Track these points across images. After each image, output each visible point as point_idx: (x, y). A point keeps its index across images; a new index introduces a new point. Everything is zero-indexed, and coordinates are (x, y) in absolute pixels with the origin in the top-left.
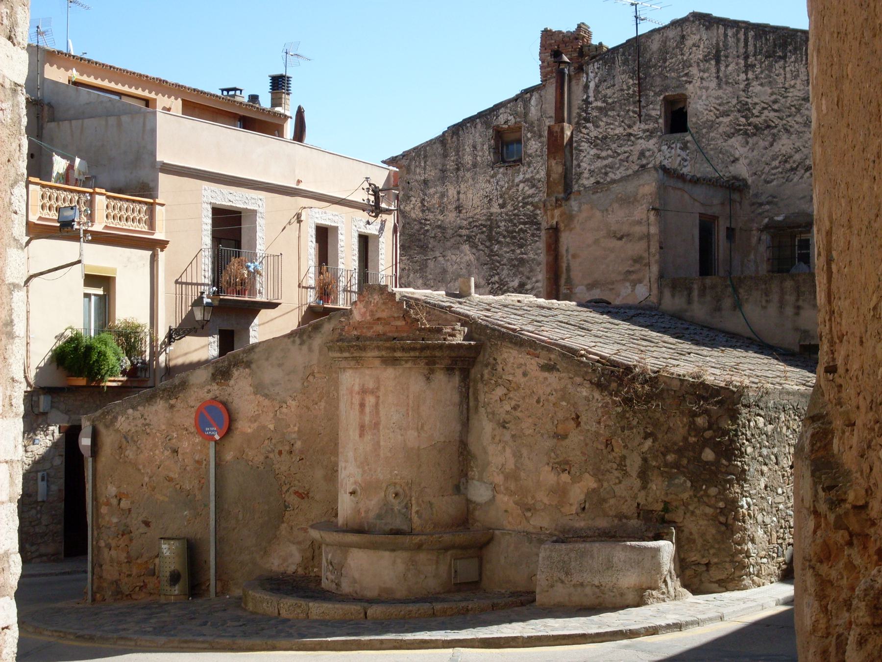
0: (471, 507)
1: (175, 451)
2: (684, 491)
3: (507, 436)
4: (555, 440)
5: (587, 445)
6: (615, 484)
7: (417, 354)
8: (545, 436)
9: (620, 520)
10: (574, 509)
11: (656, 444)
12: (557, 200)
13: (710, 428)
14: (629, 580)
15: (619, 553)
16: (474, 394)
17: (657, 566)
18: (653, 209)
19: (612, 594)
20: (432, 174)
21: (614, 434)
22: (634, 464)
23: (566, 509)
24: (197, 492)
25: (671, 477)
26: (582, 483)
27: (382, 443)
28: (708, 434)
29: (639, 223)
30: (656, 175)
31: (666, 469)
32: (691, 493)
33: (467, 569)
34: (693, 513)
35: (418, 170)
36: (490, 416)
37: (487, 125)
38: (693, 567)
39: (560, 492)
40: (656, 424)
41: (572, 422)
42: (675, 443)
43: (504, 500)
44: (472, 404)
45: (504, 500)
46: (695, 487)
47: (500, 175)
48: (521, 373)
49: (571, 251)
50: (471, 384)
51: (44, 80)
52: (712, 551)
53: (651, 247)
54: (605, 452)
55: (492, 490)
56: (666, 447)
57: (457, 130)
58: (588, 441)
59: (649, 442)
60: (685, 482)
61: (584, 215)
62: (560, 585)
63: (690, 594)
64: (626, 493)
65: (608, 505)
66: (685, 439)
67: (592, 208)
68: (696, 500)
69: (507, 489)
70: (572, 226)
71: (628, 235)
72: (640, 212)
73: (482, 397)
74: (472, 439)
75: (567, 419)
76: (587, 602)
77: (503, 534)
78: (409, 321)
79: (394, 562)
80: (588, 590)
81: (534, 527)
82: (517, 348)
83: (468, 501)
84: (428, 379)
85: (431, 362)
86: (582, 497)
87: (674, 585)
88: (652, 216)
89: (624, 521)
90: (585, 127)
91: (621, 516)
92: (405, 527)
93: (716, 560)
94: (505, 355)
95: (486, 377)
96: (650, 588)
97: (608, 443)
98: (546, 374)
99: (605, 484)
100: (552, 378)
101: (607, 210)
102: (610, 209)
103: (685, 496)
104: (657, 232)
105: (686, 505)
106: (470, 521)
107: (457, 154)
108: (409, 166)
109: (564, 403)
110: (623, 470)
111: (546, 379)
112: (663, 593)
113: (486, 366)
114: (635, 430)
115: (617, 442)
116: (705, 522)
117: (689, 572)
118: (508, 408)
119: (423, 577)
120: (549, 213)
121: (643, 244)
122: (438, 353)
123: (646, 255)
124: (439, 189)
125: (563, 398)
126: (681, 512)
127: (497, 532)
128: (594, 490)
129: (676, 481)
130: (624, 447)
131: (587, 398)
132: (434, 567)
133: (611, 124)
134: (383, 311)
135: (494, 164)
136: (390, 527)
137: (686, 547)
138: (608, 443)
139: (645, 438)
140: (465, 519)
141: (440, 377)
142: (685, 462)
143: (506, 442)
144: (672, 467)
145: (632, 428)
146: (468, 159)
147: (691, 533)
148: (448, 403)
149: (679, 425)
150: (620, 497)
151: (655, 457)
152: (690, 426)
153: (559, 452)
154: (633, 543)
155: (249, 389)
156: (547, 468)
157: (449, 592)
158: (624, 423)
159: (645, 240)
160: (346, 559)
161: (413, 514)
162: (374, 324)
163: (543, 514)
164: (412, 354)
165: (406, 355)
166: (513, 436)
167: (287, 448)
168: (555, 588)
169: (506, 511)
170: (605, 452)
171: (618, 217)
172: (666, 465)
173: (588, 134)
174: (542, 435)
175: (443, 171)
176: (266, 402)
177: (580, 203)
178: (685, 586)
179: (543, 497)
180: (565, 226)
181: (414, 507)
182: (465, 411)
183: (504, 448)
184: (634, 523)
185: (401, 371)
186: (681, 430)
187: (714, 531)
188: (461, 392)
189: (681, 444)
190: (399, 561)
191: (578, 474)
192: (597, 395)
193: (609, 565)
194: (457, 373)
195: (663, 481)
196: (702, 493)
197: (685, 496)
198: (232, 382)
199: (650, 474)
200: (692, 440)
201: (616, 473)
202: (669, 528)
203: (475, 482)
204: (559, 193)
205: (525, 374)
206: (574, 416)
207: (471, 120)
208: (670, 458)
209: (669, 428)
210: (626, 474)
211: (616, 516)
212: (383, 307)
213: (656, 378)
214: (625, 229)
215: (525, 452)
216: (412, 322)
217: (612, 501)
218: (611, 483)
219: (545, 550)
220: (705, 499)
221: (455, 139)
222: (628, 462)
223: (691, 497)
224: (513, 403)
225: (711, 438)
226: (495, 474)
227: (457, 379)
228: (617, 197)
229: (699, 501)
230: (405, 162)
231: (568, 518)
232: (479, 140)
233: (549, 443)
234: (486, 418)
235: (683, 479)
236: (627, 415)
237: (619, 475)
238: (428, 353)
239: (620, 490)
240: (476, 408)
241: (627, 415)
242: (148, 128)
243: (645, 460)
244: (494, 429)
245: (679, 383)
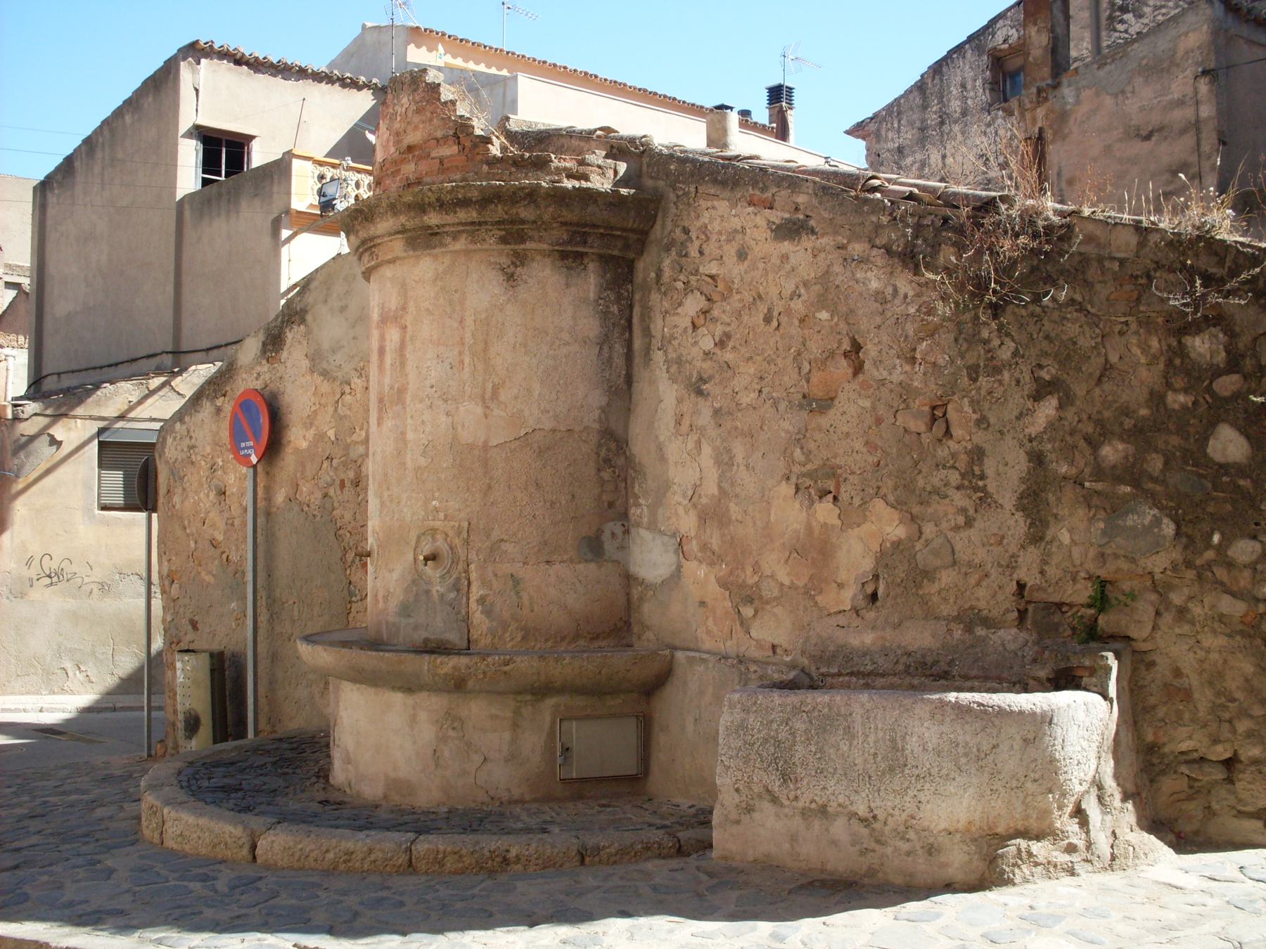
0: (636, 592)
1: (222, 493)
2: (1156, 548)
3: (705, 418)
4: (804, 414)
5: (879, 421)
6: (957, 528)
7: (473, 215)
8: (783, 406)
9: (969, 629)
10: (847, 597)
11: (1070, 414)
12: (1039, 91)
13: (1233, 365)
14: (951, 807)
15: (924, 723)
16: (642, 319)
17: (1047, 772)
18: (1204, 73)
19: (905, 846)
20: (908, 135)
21: (952, 387)
22: (1007, 470)
23: (829, 599)
25: (1115, 509)
26: (867, 527)
27: (410, 436)
28: (1227, 384)
29: (1181, 103)
30: (1209, 11)
31: (1099, 486)
32: (1176, 555)
33: (603, 744)
34: (1182, 612)
35: (890, 135)
36: (674, 369)
37: (979, 50)
38: (1184, 769)
39: (815, 552)
40: (1068, 356)
41: (844, 363)
42: (1126, 411)
43: (700, 576)
44: (638, 344)
45: (700, 576)
46: (1188, 537)
47: (1000, 121)
48: (733, 252)
49: (1066, 174)
50: (637, 297)
51: (407, 63)
52: (1243, 726)
53: (1203, 143)
54: (926, 439)
55: (676, 552)
56: (1100, 423)
57: (938, 68)
58: (882, 410)
59: (1048, 409)
60: (1157, 522)
61: (1085, 108)
62: (766, 806)
63: (1168, 852)
64: (985, 552)
65: (936, 586)
66: (1156, 399)
67: (1097, 94)
68: (1190, 574)
69: (704, 547)
70: (1066, 131)
71: (1161, 129)
72: (1180, 84)
73: (657, 326)
74: (637, 430)
75: (832, 355)
76: (842, 861)
77: (691, 660)
78: (468, 144)
79: (414, 718)
80: (839, 828)
82: (727, 194)
83: (629, 579)
84: (510, 277)
85: (513, 233)
86: (868, 565)
87: (1117, 821)
88: (1204, 86)
89: (980, 632)
90: (1122, 22)
91: (972, 619)
92: (453, 637)
93: (1255, 752)
94: (705, 217)
95: (667, 273)
96: (1025, 834)
97: (937, 415)
98: (786, 246)
99: (929, 529)
100: (799, 253)
101: (1123, 92)
102: (1129, 88)
103: (1159, 563)
104: (1213, 113)
105: (1160, 589)
106: (636, 629)
107: (941, 101)
108: (878, 130)
109: (824, 315)
110: (976, 489)
111: (785, 258)
112: (1071, 849)
113: (668, 249)
114: (1006, 375)
115: (960, 413)
116: (1221, 641)
117: (1169, 784)
118: (707, 343)
119: (478, 759)
120: (1028, 115)
121: (1189, 140)
122: (526, 213)
123: (1193, 159)
124: (919, 156)
125: (822, 301)
126: (1145, 608)
127: (680, 655)
128: (897, 544)
129: (1131, 520)
130: (978, 423)
131: (879, 297)
132: (507, 736)
133: (1162, 7)
134: (416, 128)
135: (991, 105)
136: (424, 635)
137: (1161, 711)
138: (937, 415)
139: (1037, 397)
140: (618, 621)
141: (543, 275)
142: (1156, 463)
143: (702, 430)
144: (1119, 480)
145: (997, 370)
146: (955, 105)
147: (1178, 673)
148: (566, 336)
149: (1138, 360)
150: (970, 564)
151: (1068, 452)
152: (1169, 363)
153: (812, 446)
154: (966, 697)
155: (305, 363)
156: (786, 489)
157: (548, 799)
158: (976, 355)
159: (1193, 132)
161: (473, 605)
162: (403, 161)
163: (778, 610)
164: (462, 215)
165: (449, 219)
166: (717, 412)
167: (351, 474)
168: (756, 815)
169: (702, 603)
170: (926, 439)
171: (1143, 100)
172: (1099, 473)
173: (1126, 31)
174: (775, 405)
175: (922, 129)
176: (325, 387)
177: (1078, 89)
178: (1156, 824)
179: (778, 569)
180: (1055, 134)
181: (474, 588)
182: (619, 361)
183: (698, 443)
184: (1009, 637)
185: (447, 260)
186: (1143, 373)
187: (1248, 668)
188: (605, 315)
189: (1144, 412)
190: (423, 716)
191: (857, 501)
192: (905, 283)
193: (895, 761)
194: (591, 266)
195: (1091, 520)
196: (1210, 555)
197: (1159, 563)
198: (284, 354)
199: (1051, 498)
200: (1178, 400)
201: (959, 499)
202: (1095, 653)
203: (643, 532)
204: (1043, 79)
205: (742, 255)
206: (846, 346)
207: (959, 49)
208: (1112, 452)
209: (1107, 367)
210: (985, 500)
211: (958, 619)
212: (416, 119)
213: (1069, 227)
214: (1155, 119)
215: (739, 450)
216: (475, 146)
217: (947, 578)
218: (944, 525)
219: (732, 706)
220: (1221, 573)
221: (937, 81)
222: (990, 466)
223: (1175, 567)
224: (719, 330)
225: (1237, 396)
226: (681, 511)
227: (590, 281)
228: (1139, 65)
229: (1199, 577)
230: (872, 127)
231: (833, 621)
232: (969, 74)
233: (787, 424)
234: (665, 375)
235: (1150, 513)
236: (985, 334)
237: (967, 504)
238: (499, 212)
239: (970, 544)
240: (647, 350)
241: (985, 334)
242: (509, 99)
243: (1037, 459)
244: (680, 401)
245: (1133, 240)
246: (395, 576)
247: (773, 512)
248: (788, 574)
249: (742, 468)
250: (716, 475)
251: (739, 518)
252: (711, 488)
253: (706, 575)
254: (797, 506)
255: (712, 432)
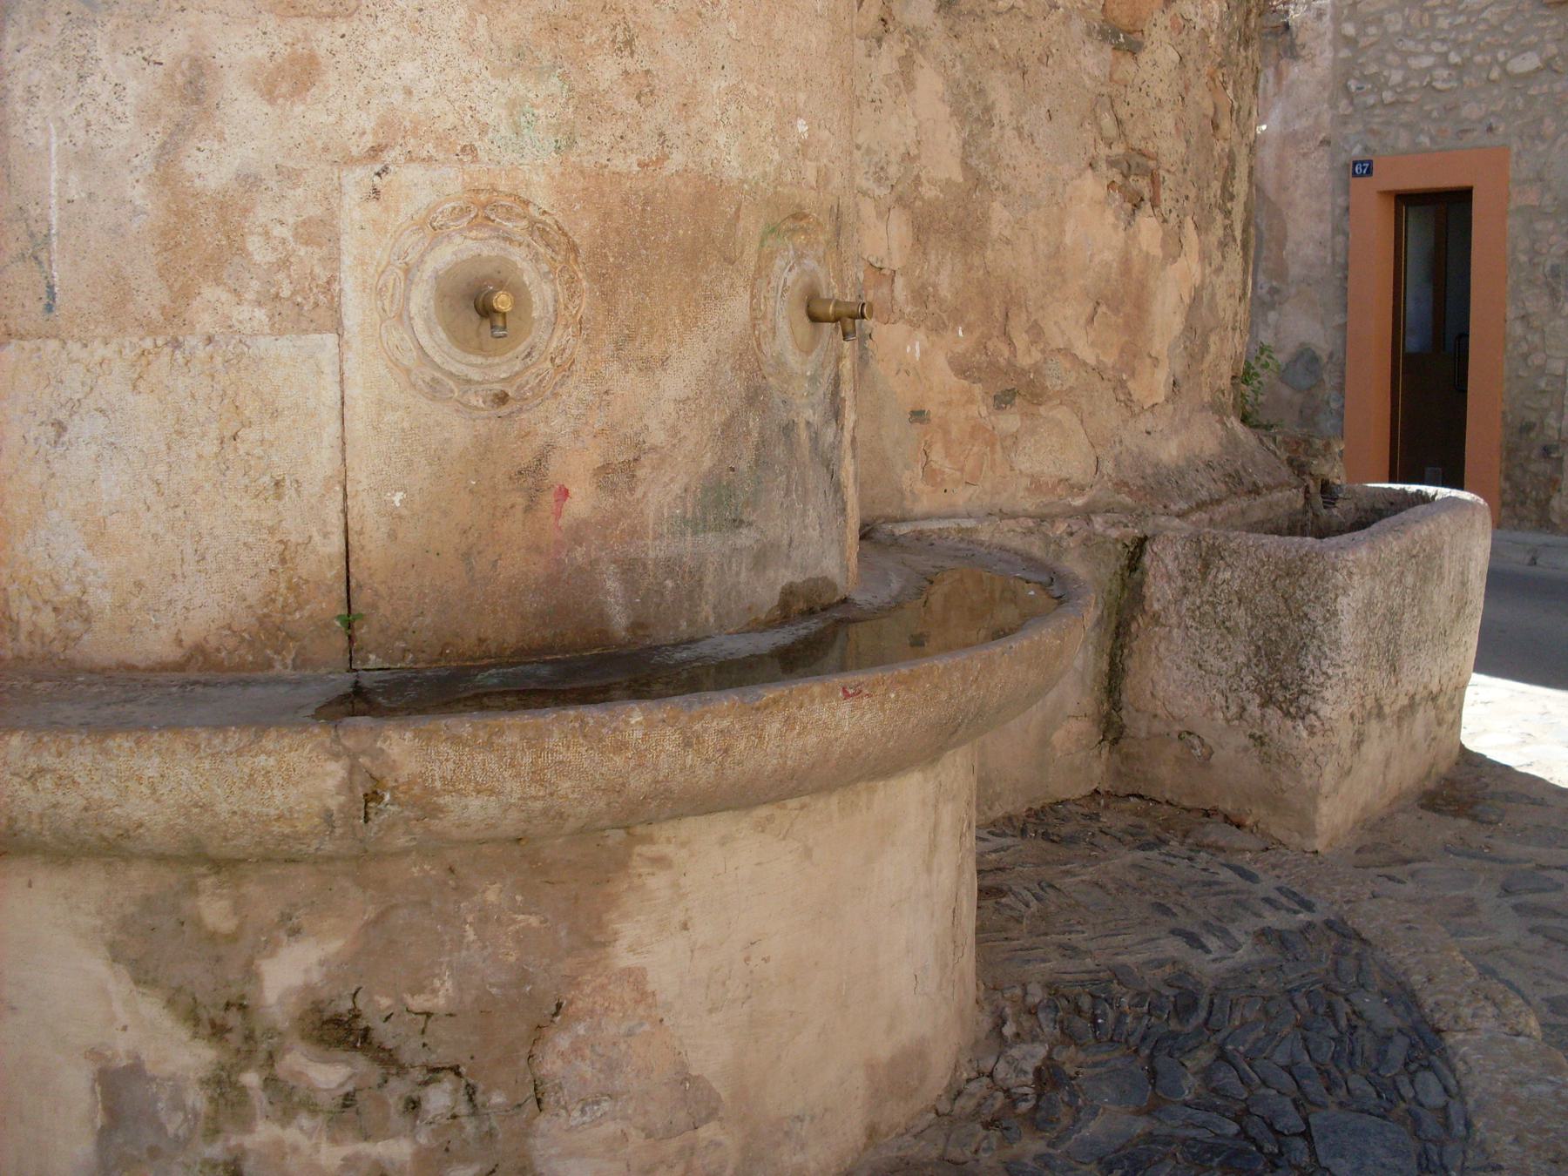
24: (108, 610)
39: (1124, 299)
69: (921, 295)
81: (1036, 485)
136: (785, 576)
156: (1091, 186)
160: (593, 939)
169: (918, 415)
179: (1072, 331)
246: (675, 383)
247: (1070, 226)
248: (1093, 344)
249: (1009, 133)
250: (955, 141)
251: (1007, 233)
252: (943, 166)
253: (924, 352)
254: (1110, 218)
255: (938, 41)
